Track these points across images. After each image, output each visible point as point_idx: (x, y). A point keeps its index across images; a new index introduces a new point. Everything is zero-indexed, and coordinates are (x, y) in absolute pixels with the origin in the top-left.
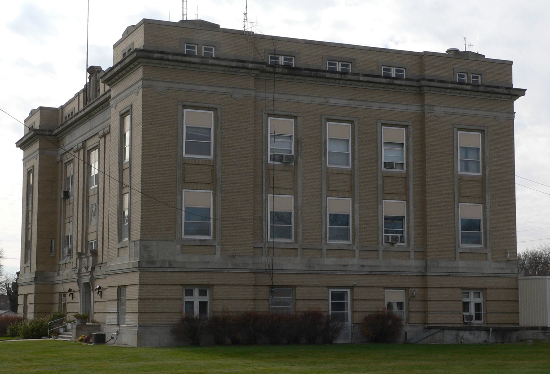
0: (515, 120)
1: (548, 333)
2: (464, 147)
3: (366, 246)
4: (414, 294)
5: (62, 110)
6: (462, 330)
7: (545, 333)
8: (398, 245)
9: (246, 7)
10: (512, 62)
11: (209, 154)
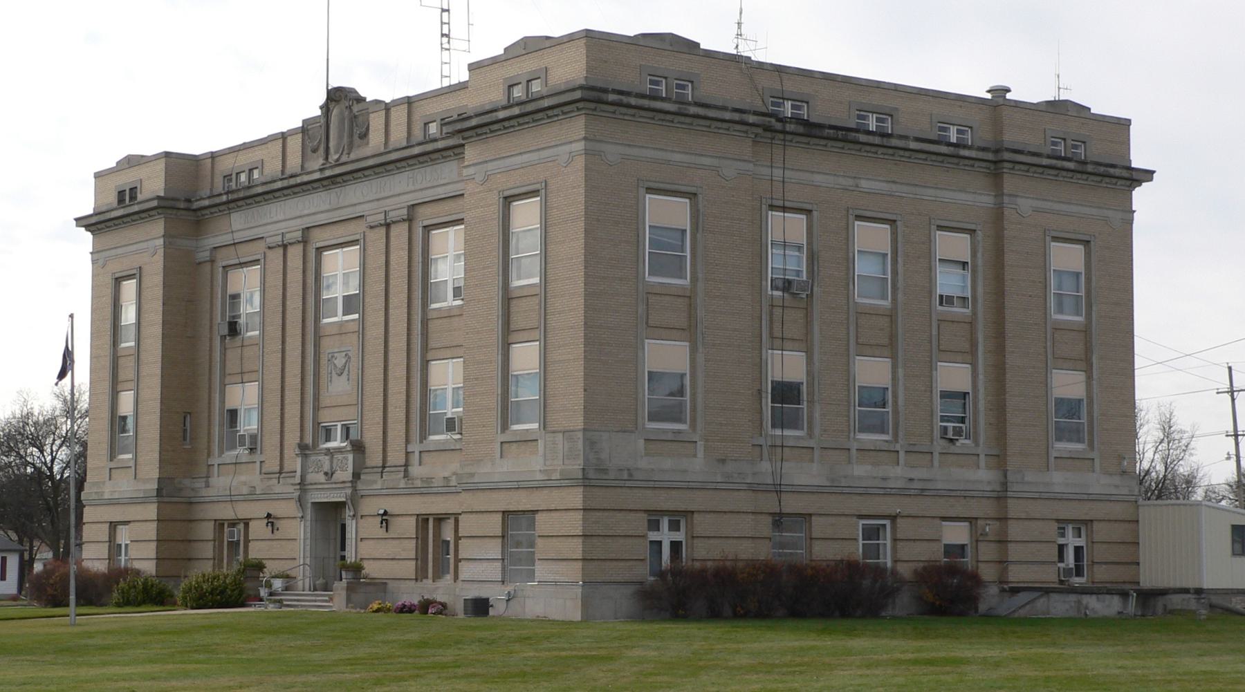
0: (1134, 225)
1: (1203, 598)
2: (880, 253)
3: (915, 445)
5: (213, 164)
6: (1086, 594)
7: (1199, 599)
9: (741, 13)
11: (683, 277)
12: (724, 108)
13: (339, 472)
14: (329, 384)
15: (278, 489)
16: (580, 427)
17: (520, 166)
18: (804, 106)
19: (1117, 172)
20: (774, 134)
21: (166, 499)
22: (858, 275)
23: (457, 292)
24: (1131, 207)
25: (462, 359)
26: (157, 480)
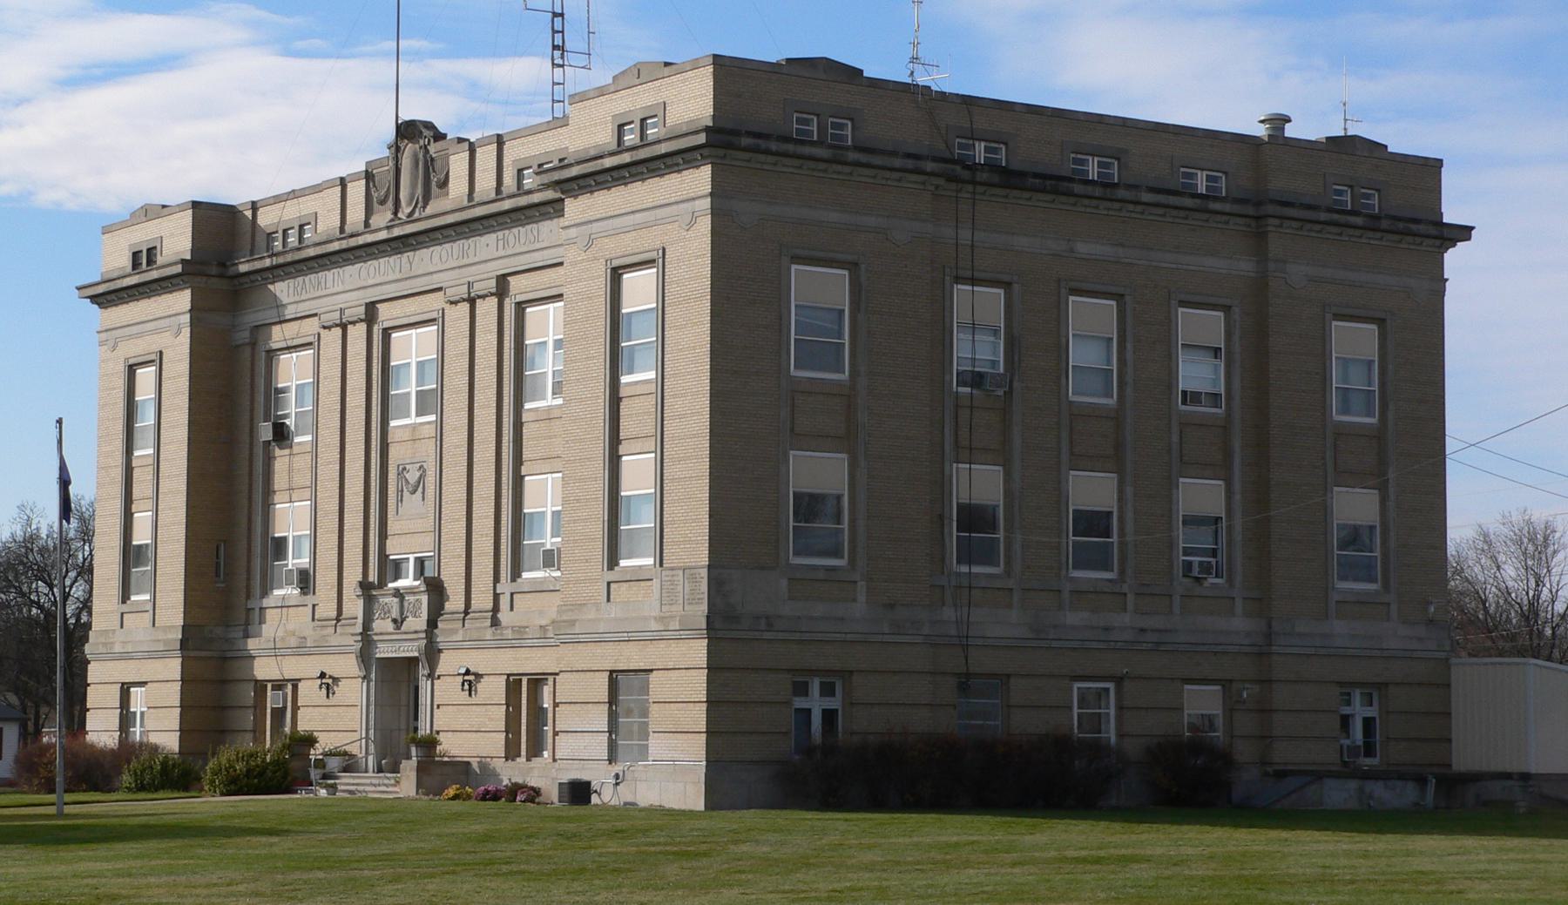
0: (1446, 298)
1: (1531, 786)
4: (1241, 696)
6: (1371, 779)
8: (1212, 584)
10: (1441, 161)
11: (841, 370)
12: (893, 154)
13: (410, 618)
14: (400, 504)
15: (334, 640)
16: (703, 563)
17: (632, 228)
18: (1001, 149)
19: (1422, 228)
20: (960, 185)
21: (192, 654)
22: (1073, 366)
23: (558, 389)
24: (1443, 276)
25: (560, 475)
26: (181, 628)
